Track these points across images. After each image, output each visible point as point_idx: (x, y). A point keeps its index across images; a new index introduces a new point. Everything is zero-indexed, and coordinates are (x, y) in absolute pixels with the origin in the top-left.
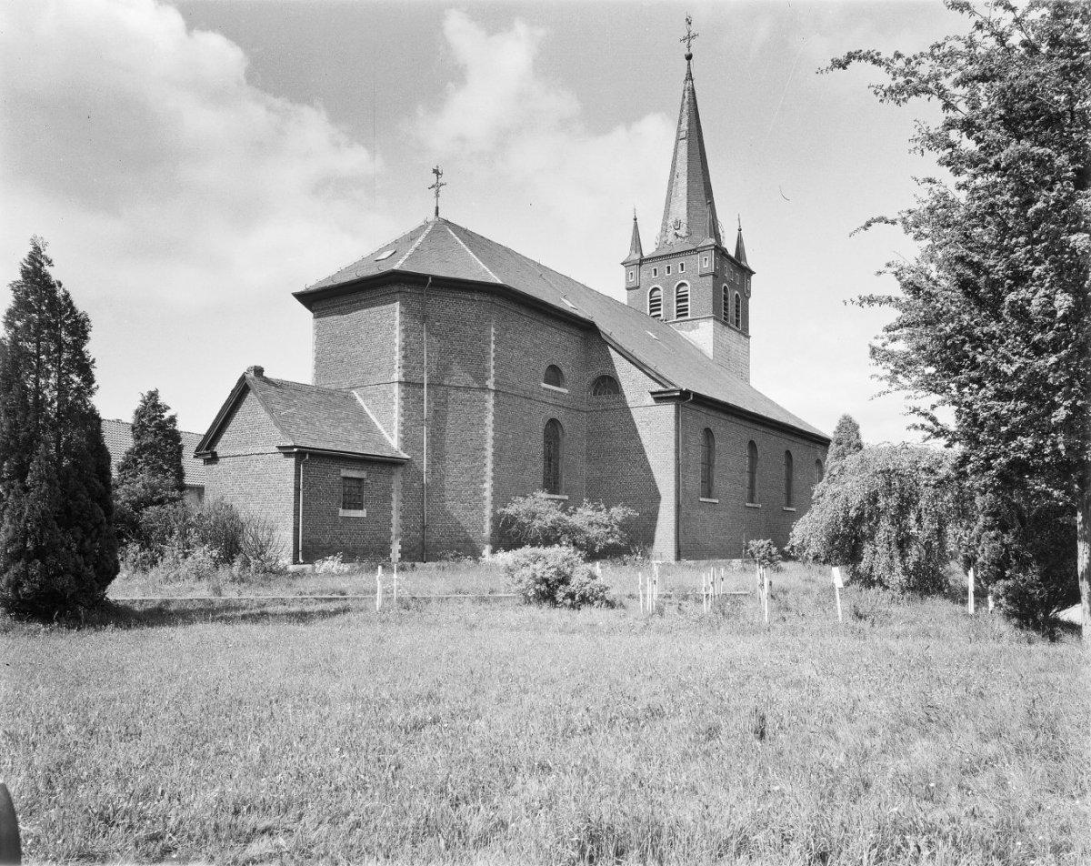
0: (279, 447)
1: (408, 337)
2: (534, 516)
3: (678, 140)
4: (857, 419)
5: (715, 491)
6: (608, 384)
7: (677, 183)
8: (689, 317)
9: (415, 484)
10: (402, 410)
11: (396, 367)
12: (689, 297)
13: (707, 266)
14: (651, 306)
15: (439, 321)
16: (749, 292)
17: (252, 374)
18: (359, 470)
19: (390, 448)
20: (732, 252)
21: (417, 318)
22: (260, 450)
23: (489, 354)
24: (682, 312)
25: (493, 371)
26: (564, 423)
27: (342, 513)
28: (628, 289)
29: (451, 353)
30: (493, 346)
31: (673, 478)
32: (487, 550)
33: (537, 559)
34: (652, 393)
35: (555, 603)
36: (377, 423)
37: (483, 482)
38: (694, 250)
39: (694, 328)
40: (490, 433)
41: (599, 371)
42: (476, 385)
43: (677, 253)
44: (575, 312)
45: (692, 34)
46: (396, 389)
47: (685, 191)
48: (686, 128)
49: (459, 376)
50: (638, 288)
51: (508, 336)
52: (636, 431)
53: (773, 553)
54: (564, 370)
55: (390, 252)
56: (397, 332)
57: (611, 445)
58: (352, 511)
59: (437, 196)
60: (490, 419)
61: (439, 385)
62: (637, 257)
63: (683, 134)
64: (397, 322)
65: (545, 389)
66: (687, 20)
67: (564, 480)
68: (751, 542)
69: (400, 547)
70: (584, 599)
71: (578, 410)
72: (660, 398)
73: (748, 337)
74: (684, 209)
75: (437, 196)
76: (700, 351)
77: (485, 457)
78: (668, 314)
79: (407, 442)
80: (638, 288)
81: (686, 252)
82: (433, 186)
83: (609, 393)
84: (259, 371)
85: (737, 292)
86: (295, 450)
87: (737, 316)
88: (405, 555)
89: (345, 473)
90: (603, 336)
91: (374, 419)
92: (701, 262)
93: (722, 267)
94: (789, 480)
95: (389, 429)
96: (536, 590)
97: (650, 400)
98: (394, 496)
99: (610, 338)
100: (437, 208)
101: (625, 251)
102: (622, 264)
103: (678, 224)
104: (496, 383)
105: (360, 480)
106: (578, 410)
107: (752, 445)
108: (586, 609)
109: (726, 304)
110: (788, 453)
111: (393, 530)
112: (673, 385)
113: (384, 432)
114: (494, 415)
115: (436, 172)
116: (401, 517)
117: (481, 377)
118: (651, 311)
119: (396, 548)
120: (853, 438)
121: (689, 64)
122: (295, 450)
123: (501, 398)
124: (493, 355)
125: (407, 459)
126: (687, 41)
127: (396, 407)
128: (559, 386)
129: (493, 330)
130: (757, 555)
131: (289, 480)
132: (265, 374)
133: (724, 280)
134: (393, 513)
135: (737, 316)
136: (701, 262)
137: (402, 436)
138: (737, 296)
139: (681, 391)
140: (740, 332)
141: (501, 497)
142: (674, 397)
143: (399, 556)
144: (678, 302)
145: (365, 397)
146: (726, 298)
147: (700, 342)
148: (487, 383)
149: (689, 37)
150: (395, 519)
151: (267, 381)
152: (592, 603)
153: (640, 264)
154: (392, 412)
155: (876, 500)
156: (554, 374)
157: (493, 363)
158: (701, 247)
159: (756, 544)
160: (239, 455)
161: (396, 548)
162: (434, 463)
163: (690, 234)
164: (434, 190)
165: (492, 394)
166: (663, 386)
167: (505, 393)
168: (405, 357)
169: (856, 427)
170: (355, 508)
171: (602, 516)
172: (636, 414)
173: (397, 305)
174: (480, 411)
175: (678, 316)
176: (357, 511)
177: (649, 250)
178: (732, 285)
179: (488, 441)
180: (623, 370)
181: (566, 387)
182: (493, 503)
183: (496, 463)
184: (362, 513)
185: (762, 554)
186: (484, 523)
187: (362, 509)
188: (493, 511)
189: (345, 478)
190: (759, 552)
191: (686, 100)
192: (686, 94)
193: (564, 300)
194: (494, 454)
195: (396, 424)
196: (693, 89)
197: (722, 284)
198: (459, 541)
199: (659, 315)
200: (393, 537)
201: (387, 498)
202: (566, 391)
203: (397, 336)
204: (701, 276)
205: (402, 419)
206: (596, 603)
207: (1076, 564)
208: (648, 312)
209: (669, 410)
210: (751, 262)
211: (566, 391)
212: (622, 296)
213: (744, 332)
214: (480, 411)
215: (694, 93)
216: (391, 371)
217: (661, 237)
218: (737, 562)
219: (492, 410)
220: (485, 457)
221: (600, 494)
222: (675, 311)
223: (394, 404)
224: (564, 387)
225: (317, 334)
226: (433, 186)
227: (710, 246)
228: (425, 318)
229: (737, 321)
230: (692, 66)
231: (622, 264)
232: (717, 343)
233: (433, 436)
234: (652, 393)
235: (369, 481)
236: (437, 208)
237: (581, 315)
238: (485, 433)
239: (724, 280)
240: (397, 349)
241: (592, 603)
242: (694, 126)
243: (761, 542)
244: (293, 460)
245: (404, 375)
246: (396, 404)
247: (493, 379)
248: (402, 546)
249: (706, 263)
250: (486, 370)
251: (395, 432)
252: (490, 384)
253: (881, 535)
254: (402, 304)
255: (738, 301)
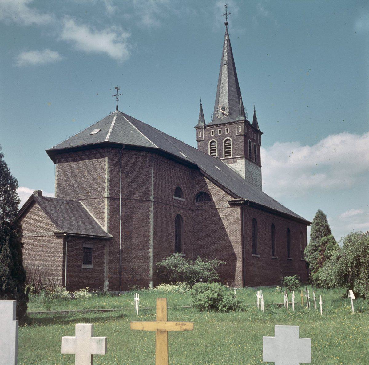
0: (55, 233)
1: (111, 174)
2: (176, 266)
3: (222, 65)
4: (325, 212)
5: (258, 251)
6: (205, 196)
7: (222, 87)
8: (232, 157)
9: (116, 250)
10: (109, 212)
11: (106, 190)
12: (232, 146)
13: (241, 131)
14: (211, 150)
15: (127, 167)
16: (260, 143)
17: (37, 195)
18: (90, 243)
19: (103, 232)
20: (251, 123)
21: (115, 167)
22: (42, 234)
23: (151, 183)
24: (228, 154)
25: (153, 192)
26: (183, 216)
27: (83, 266)
28: (198, 141)
29: (133, 182)
30: (153, 179)
31: (241, 245)
32: (151, 285)
33: (207, 289)
34: (229, 201)
35: (217, 309)
36: (95, 219)
37: (149, 248)
38: (234, 122)
39: (234, 162)
40: (152, 223)
41: (199, 189)
42: (145, 199)
43: (223, 124)
44: (188, 160)
45: (228, 13)
46: (106, 201)
47: (227, 91)
48: (227, 59)
49: (138, 195)
50: (203, 140)
51: (159, 173)
52: (220, 220)
53: (297, 283)
54: (183, 189)
55: (98, 130)
56: (106, 172)
57: (207, 227)
58: (87, 265)
59: (117, 100)
60: (152, 216)
61: (127, 199)
62: (203, 124)
63: (225, 62)
64: (106, 167)
65: (175, 199)
66: (225, 6)
67: (183, 247)
68: (285, 278)
69: (108, 283)
70: (231, 308)
71: (189, 210)
72: (232, 204)
73: (261, 166)
74: (227, 101)
75: (117, 100)
76: (238, 175)
77: (149, 236)
78: (220, 155)
79: (112, 227)
80: (203, 140)
81: (229, 123)
82: (115, 95)
83: (205, 201)
84: (40, 193)
85: (255, 144)
86: (65, 234)
87: (255, 156)
88: (111, 287)
89: (85, 245)
90: (202, 172)
91: (93, 217)
92: (238, 128)
93: (248, 131)
94: (288, 243)
95: (102, 221)
96: (209, 304)
97: (227, 205)
98: (105, 257)
99: (206, 173)
100: (117, 107)
101: (196, 121)
102: (195, 128)
103: (224, 108)
104: (154, 197)
105: (90, 249)
106: (189, 210)
107: (273, 225)
108: (231, 312)
109: (250, 150)
110: (288, 229)
111: (105, 274)
112: (240, 197)
113: (99, 223)
114: (154, 214)
115: (117, 88)
116: (109, 268)
117: (147, 195)
118: (211, 153)
119: (106, 283)
120: (324, 222)
121: (227, 27)
122: (65, 234)
123: (157, 205)
124: (153, 183)
125: (112, 237)
126: (225, 17)
127: (106, 211)
128: (180, 197)
129: (153, 171)
130: (289, 284)
131: (60, 250)
132: (43, 195)
133: (249, 138)
134: (105, 265)
135: (255, 156)
136: (238, 128)
137: (109, 225)
138: (255, 145)
139: (244, 200)
140: (257, 164)
141: (158, 257)
142: (241, 203)
143: (107, 288)
144: (225, 149)
145: (87, 205)
146: (250, 147)
147: (237, 170)
148: (151, 198)
149: (226, 14)
150: (106, 269)
151: (44, 198)
152: (235, 310)
153: (205, 128)
154: (104, 213)
155: (359, 259)
156: (178, 192)
157: (153, 187)
158: (237, 121)
159: (288, 279)
160: (28, 237)
161: (106, 283)
162: (125, 239)
163: (230, 113)
164: (115, 97)
165: (153, 204)
166: (234, 198)
167: (158, 203)
168: (110, 185)
169: (325, 217)
170: (88, 264)
171: (208, 265)
172: (221, 213)
173: (106, 159)
174: (147, 212)
175: (226, 156)
176: (89, 265)
177: (208, 121)
178: (253, 140)
179: (151, 227)
180: (212, 188)
181: (184, 198)
182: (154, 259)
183: (154, 238)
184: (91, 266)
185: (291, 283)
186: (149, 270)
187: (91, 264)
188: (154, 263)
189: (84, 248)
190: (290, 283)
191: (226, 45)
192: (226, 42)
193: (180, 153)
194: (154, 234)
195: (106, 219)
196: (229, 40)
197: (248, 140)
198: (137, 280)
199: (216, 155)
200: (105, 278)
201: (102, 258)
202: (184, 200)
203: (107, 174)
204: (238, 136)
205: (109, 216)
206: (237, 309)
207: (228, 241)
208: (209, 154)
209: (238, 210)
210: (261, 128)
211: (184, 200)
212: (194, 144)
213: (259, 165)
214: (147, 212)
215: (230, 42)
216: (104, 192)
217: (215, 114)
218: (278, 288)
219: (153, 211)
220: (149, 236)
221: (207, 256)
222: (224, 153)
223: (105, 209)
224: (183, 198)
225: (58, 171)
226: (115, 95)
227: (242, 120)
228: (120, 166)
229: (256, 159)
230: (228, 28)
231: (195, 128)
232: (247, 171)
233: (125, 225)
234: (229, 201)
235: (94, 249)
236: (117, 107)
237: (191, 161)
238: (150, 223)
239: (249, 138)
240: (106, 181)
241: (235, 310)
242: (230, 58)
243: (290, 278)
244: (62, 239)
245: (110, 194)
246: (106, 209)
247: (153, 196)
248: (109, 283)
249: (240, 129)
250: (150, 191)
251: (106, 223)
252: (152, 198)
253: (362, 275)
254: (109, 158)
255: (255, 148)
